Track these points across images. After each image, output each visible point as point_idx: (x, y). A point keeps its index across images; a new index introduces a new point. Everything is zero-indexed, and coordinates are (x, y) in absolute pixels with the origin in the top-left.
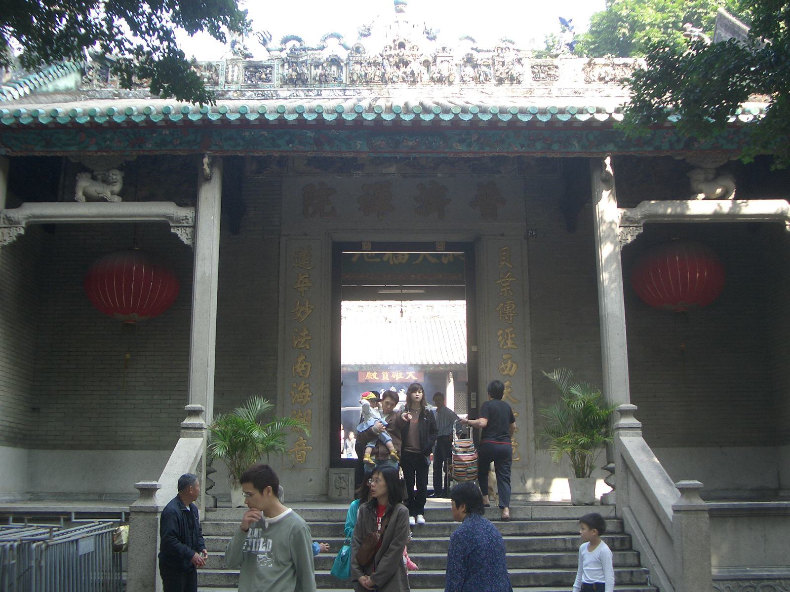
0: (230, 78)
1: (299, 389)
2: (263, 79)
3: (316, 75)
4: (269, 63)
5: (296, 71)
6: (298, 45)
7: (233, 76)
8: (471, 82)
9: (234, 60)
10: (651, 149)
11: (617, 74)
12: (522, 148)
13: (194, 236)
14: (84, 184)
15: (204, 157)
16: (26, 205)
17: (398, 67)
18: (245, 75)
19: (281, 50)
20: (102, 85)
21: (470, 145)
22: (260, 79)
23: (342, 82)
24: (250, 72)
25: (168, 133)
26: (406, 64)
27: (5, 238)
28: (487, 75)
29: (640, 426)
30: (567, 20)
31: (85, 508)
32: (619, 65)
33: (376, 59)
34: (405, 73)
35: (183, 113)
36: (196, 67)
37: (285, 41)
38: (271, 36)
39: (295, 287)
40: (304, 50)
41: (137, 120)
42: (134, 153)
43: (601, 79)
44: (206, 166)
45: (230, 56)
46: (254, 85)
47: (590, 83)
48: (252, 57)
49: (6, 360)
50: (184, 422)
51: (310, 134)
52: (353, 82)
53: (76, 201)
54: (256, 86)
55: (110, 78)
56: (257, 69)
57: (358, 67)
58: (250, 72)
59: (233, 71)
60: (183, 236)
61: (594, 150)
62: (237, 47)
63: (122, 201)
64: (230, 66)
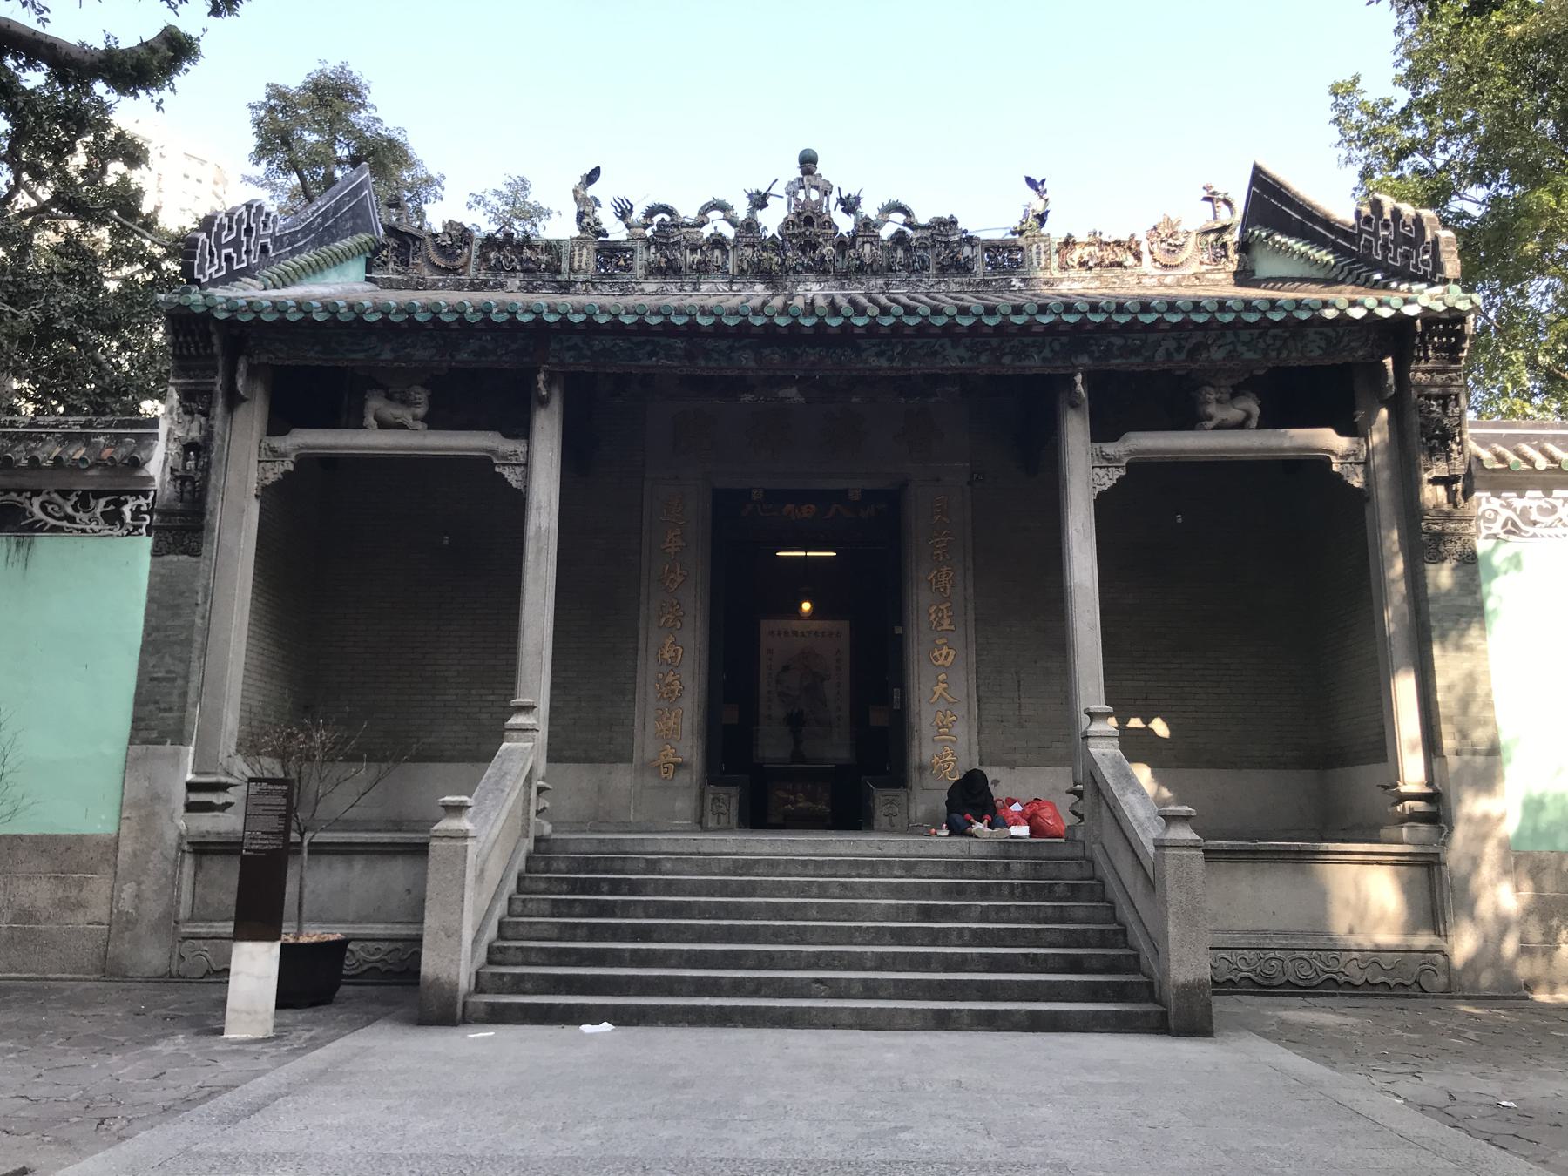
0: (576, 264)
1: (667, 681)
2: (621, 266)
3: (693, 261)
4: (629, 245)
5: (666, 257)
6: (667, 218)
7: (580, 261)
8: (903, 272)
9: (582, 239)
10: (1139, 360)
11: (1105, 256)
12: (961, 362)
13: (526, 478)
14: (375, 404)
15: (539, 372)
16: (295, 431)
17: (803, 252)
18: (597, 261)
19: (646, 227)
20: (400, 269)
21: (891, 359)
22: (617, 266)
23: (728, 272)
24: (604, 256)
25: (489, 338)
26: (815, 247)
27: (267, 475)
28: (924, 261)
29: (1118, 734)
30: (1039, 181)
31: (372, 838)
32: (1108, 244)
33: (1544, 504)
34: (812, 259)
35: (509, 312)
36: (530, 247)
37: (651, 212)
38: (632, 206)
39: (663, 547)
40: (676, 226)
41: (447, 319)
42: (444, 365)
43: (1082, 264)
44: (541, 385)
45: (577, 233)
46: (609, 275)
47: (1066, 269)
48: (607, 236)
49: (268, 640)
50: (510, 722)
51: (679, 344)
52: (742, 272)
53: (365, 428)
54: (611, 276)
55: (411, 262)
56: (612, 252)
57: (749, 251)
58: (604, 256)
59: (581, 255)
60: (512, 476)
61: (1059, 364)
62: (585, 220)
63: (429, 429)
64: (577, 248)
